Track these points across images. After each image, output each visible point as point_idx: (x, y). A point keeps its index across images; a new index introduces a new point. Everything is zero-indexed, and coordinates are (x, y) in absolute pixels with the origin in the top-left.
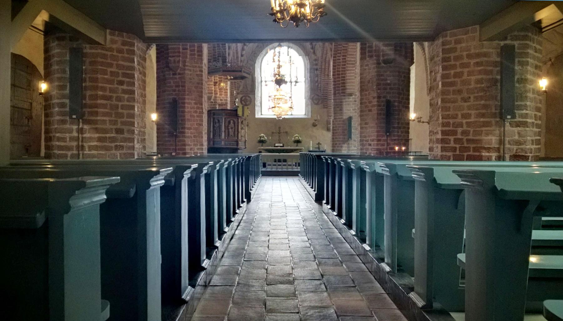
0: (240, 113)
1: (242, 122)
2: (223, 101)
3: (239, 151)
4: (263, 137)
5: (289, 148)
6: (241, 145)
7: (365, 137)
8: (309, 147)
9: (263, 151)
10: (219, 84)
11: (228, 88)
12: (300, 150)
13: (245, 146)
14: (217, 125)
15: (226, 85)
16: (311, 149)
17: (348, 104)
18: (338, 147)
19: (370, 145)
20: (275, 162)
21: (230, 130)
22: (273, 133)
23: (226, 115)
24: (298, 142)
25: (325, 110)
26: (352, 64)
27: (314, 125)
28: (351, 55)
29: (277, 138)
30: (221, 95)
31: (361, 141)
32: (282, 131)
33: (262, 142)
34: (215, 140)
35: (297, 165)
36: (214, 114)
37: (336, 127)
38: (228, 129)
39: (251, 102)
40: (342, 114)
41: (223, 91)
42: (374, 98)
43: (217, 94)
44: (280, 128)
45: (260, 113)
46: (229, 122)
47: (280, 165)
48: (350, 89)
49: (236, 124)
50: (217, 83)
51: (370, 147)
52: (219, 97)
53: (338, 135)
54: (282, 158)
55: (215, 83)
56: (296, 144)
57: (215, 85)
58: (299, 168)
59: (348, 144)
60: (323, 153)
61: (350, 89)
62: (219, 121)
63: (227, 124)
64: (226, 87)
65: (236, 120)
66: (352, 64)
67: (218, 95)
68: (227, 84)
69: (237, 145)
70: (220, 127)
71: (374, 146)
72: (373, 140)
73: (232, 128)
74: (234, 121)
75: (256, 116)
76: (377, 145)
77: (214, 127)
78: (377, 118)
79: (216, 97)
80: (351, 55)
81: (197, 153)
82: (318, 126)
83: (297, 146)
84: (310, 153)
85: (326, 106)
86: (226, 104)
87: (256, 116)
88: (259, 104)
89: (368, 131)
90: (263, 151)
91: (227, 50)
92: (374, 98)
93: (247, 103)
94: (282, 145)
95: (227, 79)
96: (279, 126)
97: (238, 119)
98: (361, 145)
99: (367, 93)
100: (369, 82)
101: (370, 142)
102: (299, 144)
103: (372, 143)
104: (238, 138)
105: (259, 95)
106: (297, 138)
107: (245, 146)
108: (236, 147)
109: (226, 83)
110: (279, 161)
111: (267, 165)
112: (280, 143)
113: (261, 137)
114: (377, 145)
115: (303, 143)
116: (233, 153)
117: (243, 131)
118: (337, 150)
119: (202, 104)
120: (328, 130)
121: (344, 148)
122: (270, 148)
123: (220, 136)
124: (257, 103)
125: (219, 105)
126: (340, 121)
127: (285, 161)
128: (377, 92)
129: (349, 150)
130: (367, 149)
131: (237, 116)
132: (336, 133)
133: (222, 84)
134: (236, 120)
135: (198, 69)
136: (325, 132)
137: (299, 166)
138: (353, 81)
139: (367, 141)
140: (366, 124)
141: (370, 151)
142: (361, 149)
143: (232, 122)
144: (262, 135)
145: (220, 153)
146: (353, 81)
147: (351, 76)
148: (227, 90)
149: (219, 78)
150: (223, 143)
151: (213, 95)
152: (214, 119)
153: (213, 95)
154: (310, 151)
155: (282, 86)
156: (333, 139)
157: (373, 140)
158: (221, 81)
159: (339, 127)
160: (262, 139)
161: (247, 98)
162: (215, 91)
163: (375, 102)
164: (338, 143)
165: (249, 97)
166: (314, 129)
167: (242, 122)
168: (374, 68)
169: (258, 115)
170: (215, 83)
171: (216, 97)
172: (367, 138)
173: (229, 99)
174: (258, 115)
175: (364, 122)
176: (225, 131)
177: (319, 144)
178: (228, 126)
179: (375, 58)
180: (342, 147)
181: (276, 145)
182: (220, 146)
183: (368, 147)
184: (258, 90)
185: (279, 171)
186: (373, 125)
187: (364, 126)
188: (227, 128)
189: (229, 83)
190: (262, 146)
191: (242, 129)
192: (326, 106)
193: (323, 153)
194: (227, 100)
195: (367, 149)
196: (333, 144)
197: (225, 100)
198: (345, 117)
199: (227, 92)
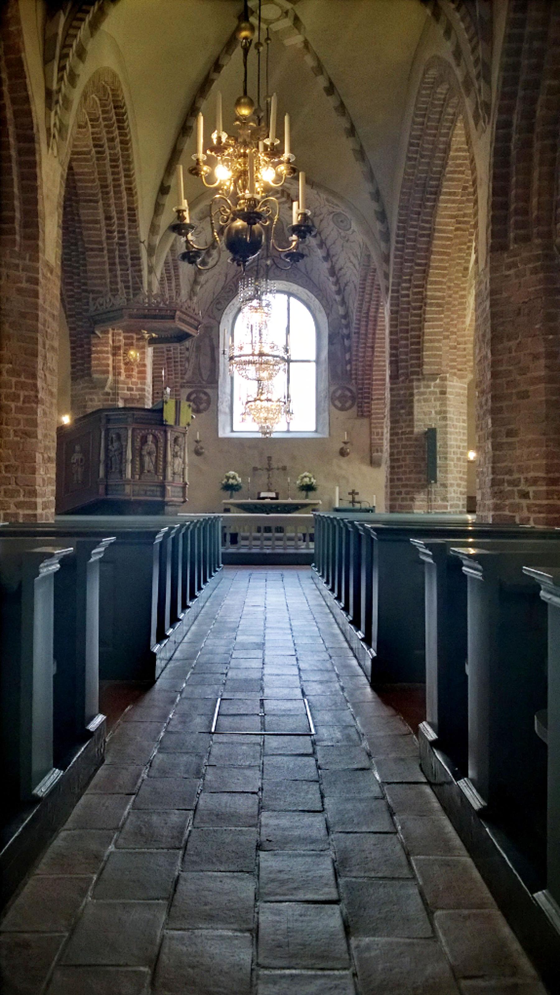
0: (169, 416)
1: (176, 440)
2: (134, 392)
3: (168, 509)
4: (234, 478)
5: (290, 501)
6: (172, 494)
7: (510, 472)
8: (331, 502)
9: (232, 508)
10: (126, 353)
11: (149, 361)
12: (314, 508)
13: (184, 496)
14: (116, 445)
15: (143, 356)
16: (337, 505)
17: (426, 400)
18: (403, 499)
19: (525, 495)
20: (259, 531)
21: (147, 459)
22: (255, 469)
23: (136, 421)
24: (309, 488)
25: (365, 421)
26: (438, 305)
27: (343, 453)
28: (436, 283)
29: (264, 479)
30: (129, 376)
31: (494, 483)
32: (274, 465)
33: (229, 488)
34: (111, 482)
35: (308, 538)
36: (108, 421)
37: (399, 453)
38: (141, 456)
39: (209, 402)
40: (411, 423)
41: (133, 369)
42: (536, 357)
43: (119, 374)
44: (270, 458)
45: (228, 429)
46: (144, 441)
47: (268, 539)
48: (429, 364)
49: (161, 444)
50: (119, 348)
51: (524, 502)
52: (124, 383)
53: (405, 473)
54: (273, 525)
55: (116, 350)
56: (304, 493)
57: (114, 355)
58: (312, 545)
59: (429, 493)
60: (370, 516)
61: (429, 364)
62: (119, 437)
63: (138, 444)
64: (143, 359)
65: (160, 435)
66: (438, 305)
67: (122, 378)
68: (143, 353)
69: (163, 493)
70: (122, 452)
71: (535, 498)
72: (534, 481)
73: (149, 454)
74: (155, 437)
75: (221, 434)
76: (549, 494)
77: (107, 450)
78: (547, 417)
79: (116, 382)
80: (436, 283)
81: (16, 515)
82: (352, 455)
83: (307, 497)
84: (339, 516)
85: (364, 413)
86: (142, 398)
87: (221, 434)
88: (227, 410)
89: (518, 452)
90: (232, 508)
91: (145, 273)
92: (536, 357)
93: (202, 407)
94: (273, 495)
95: (143, 338)
96: (267, 453)
97: (166, 432)
98: (494, 495)
99: (513, 344)
100: (519, 314)
101: (523, 487)
102: (311, 494)
103: (531, 489)
104: (165, 477)
105: (228, 390)
106: (307, 480)
107: (184, 496)
108: (160, 499)
109: (142, 349)
110: (268, 529)
111: (239, 538)
112: (269, 490)
113: (228, 478)
114: (549, 494)
115: (318, 492)
116: (156, 513)
117: (178, 461)
118: (401, 507)
119: (34, 376)
120: (374, 463)
121: (417, 503)
122: (250, 501)
123: (122, 472)
124: (223, 407)
125: (126, 400)
126: (408, 439)
127: (280, 530)
128: (545, 340)
129: (430, 507)
130: (516, 508)
131: (162, 423)
132: (400, 467)
133: (132, 353)
134: (160, 435)
135: (24, 275)
136: (366, 469)
137: (312, 540)
138: (436, 344)
139: (514, 483)
140: (510, 433)
141: (525, 513)
142: (497, 507)
143: (150, 438)
144: (232, 473)
145: (121, 513)
146: (436, 344)
147: (435, 334)
148: (144, 365)
149: (126, 338)
150: (128, 489)
151: (111, 377)
152: (107, 431)
153: (111, 377)
154: (337, 510)
155: (274, 367)
156: (392, 480)
157: (534, 481)
158: (129, 345)
159: (407, 453)
160: (231, 481)
161: (202, 396)
162: (114, 368)
163: (539, 369)
164: (403, 490)
165: (205, 394)
166: (343, 462)
167: (176, 440)
168: (535, 271)
169: (224, 433)
170: (116, 350)
171: (116, 382)
172: (516, 476)
173: (149, 388)
174: (224, 433)
175: (503, 430)
176: (133, 461)
177: (353, 493)
178: (141, 449)
179: (538, 241)
180: (412, 499)
181: (263, 495)
182: (122, 497)
183: (517, 500)
184: (224, 378)
185: (265, 554)
186: (530, 437)
187: (505, 440)
188: (138, 453)
189: (150, 351)
190: (231, 497)
191: (175, 455)
192: (364, 413)
193: (370, 516)
194: (143, 390)
195: (516, 508)
196: (392, 493)
197: (138, 389)
198: (419, 428)
199: (144, 372)
